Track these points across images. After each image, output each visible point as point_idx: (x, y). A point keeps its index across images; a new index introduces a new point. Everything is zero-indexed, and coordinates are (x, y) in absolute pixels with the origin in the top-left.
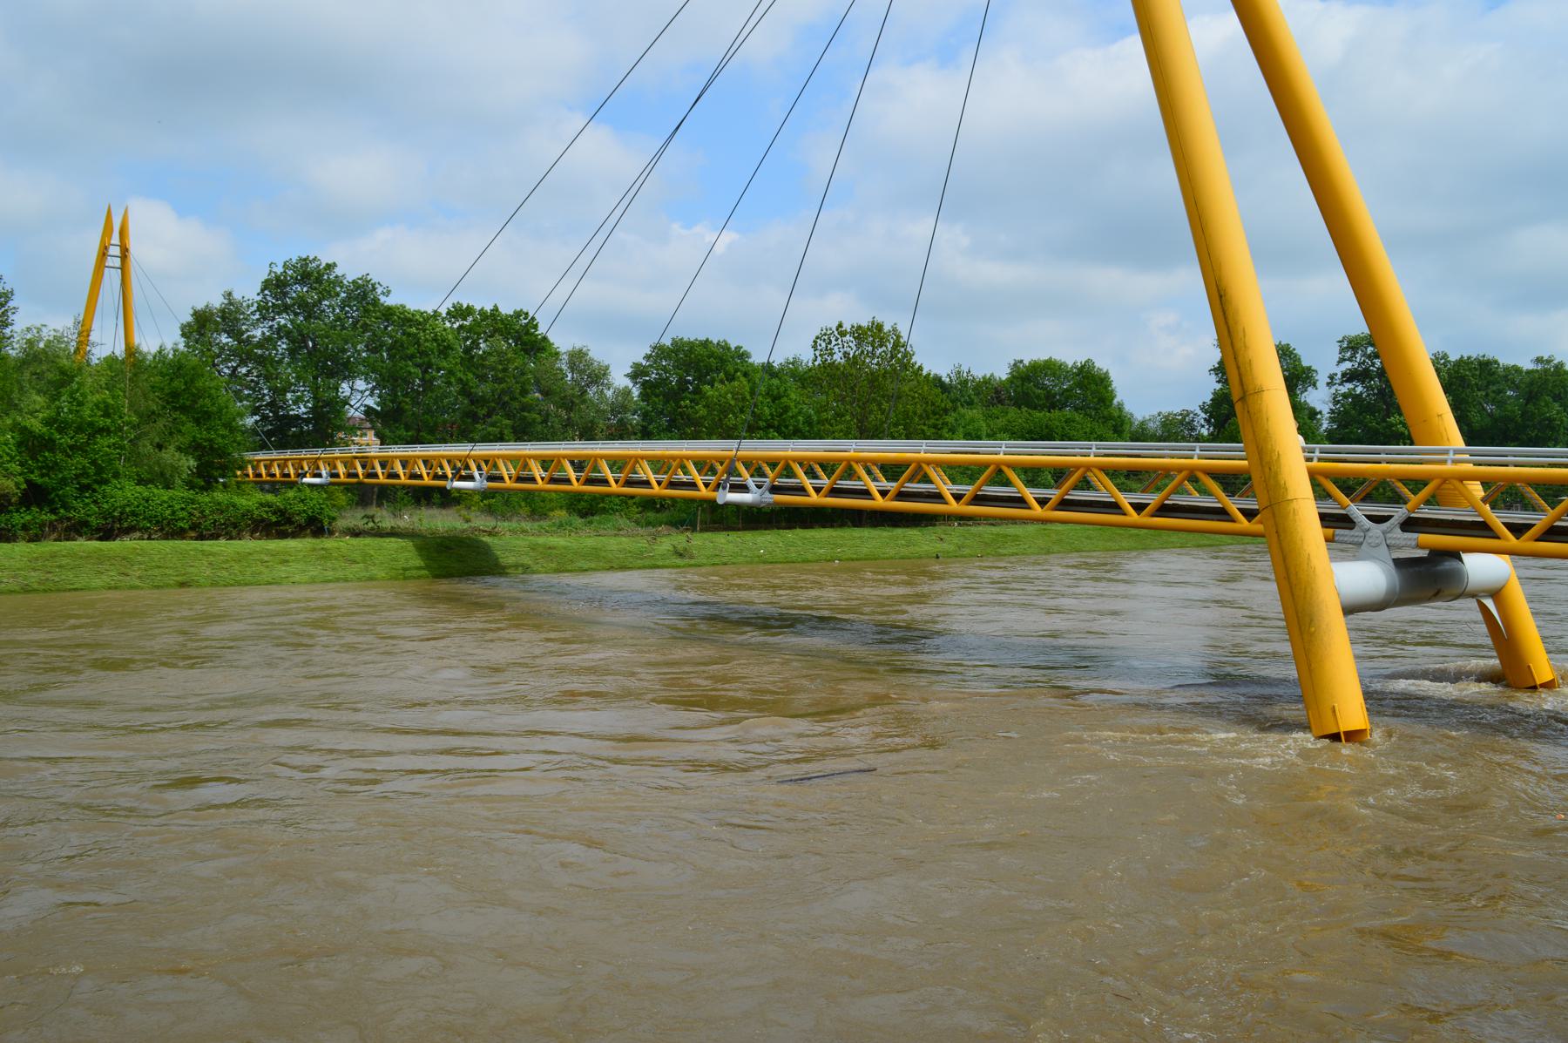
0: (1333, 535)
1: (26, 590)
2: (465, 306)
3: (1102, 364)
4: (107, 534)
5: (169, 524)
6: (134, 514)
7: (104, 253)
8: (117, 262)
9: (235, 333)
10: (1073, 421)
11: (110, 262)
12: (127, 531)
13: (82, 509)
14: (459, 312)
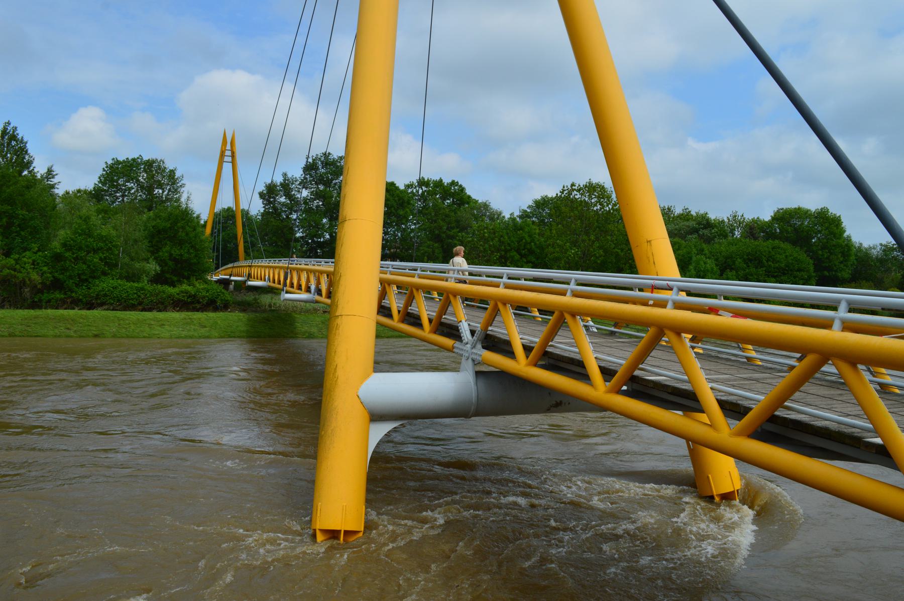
0: (453, 347)
1: (11, 335)
2: (426, 179)
3: (834, 210)
4: (90, 306)
5: (125, 301)
6: (105, 295)
7: (222, 155)
8: (230, 159)
9: (288, 195)
10: (779, 248)
11: (226, 159)
12: (101, 305)
13: (80, 293)
14: (422, 183)
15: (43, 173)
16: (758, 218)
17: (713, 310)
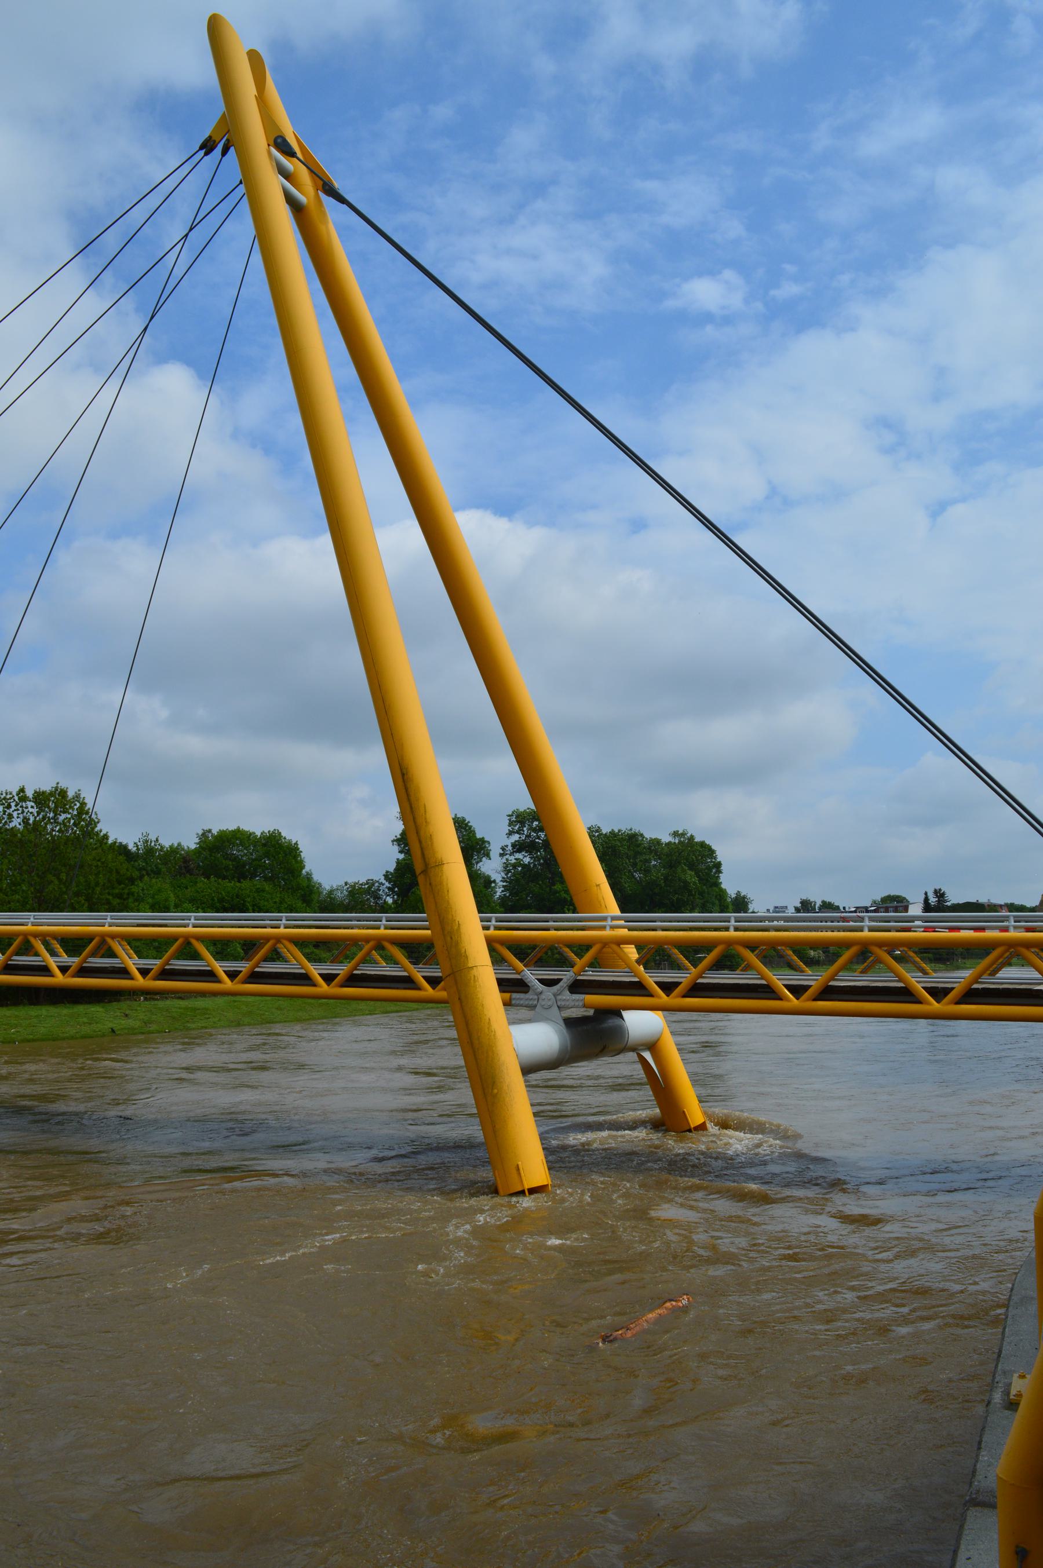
15: (482, 869)
16: (179, 844)
17: (654, 929)
